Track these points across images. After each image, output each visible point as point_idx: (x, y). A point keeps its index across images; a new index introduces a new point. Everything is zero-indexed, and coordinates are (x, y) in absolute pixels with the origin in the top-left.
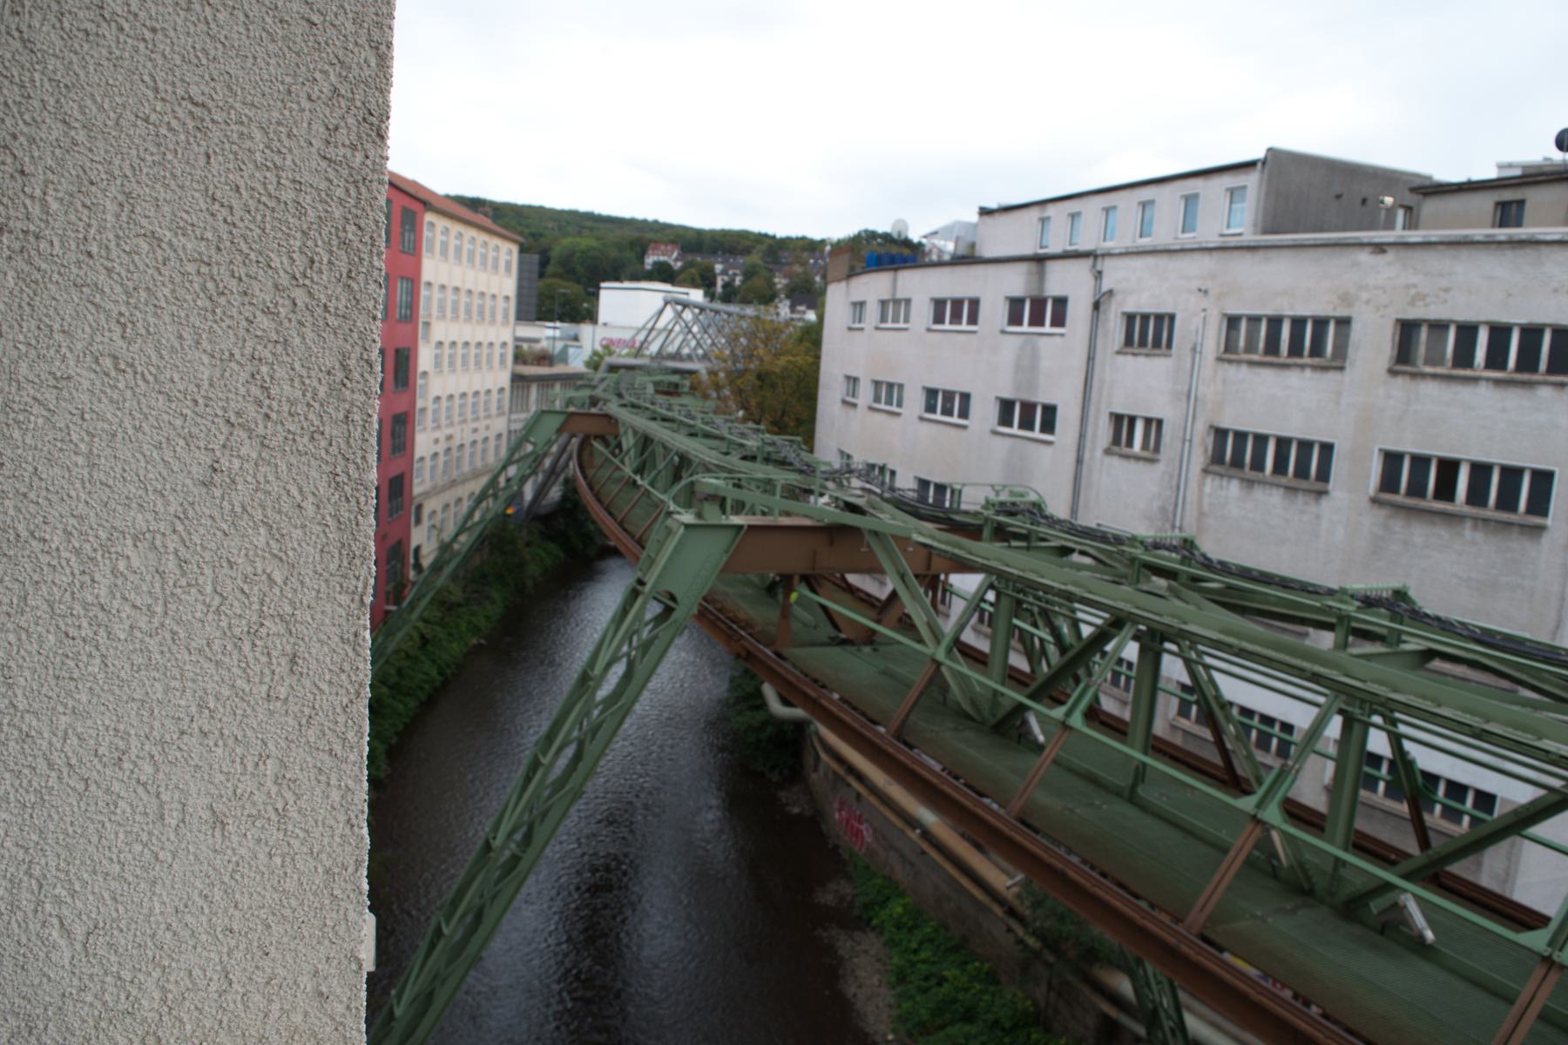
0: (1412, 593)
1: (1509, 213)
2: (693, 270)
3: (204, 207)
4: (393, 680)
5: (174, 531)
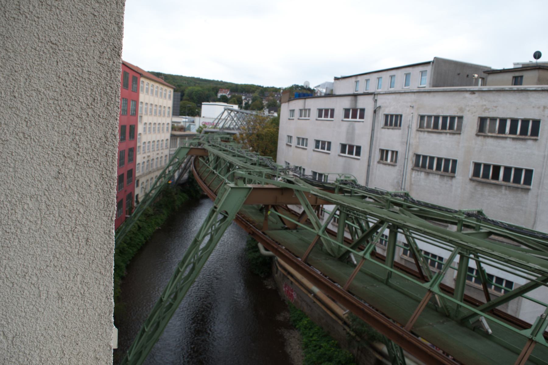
0: (484, 212)
1: (517, 80)
2: (235, 98)
3: (56, 80)
4: (128, 241)
5: (45, 195)
